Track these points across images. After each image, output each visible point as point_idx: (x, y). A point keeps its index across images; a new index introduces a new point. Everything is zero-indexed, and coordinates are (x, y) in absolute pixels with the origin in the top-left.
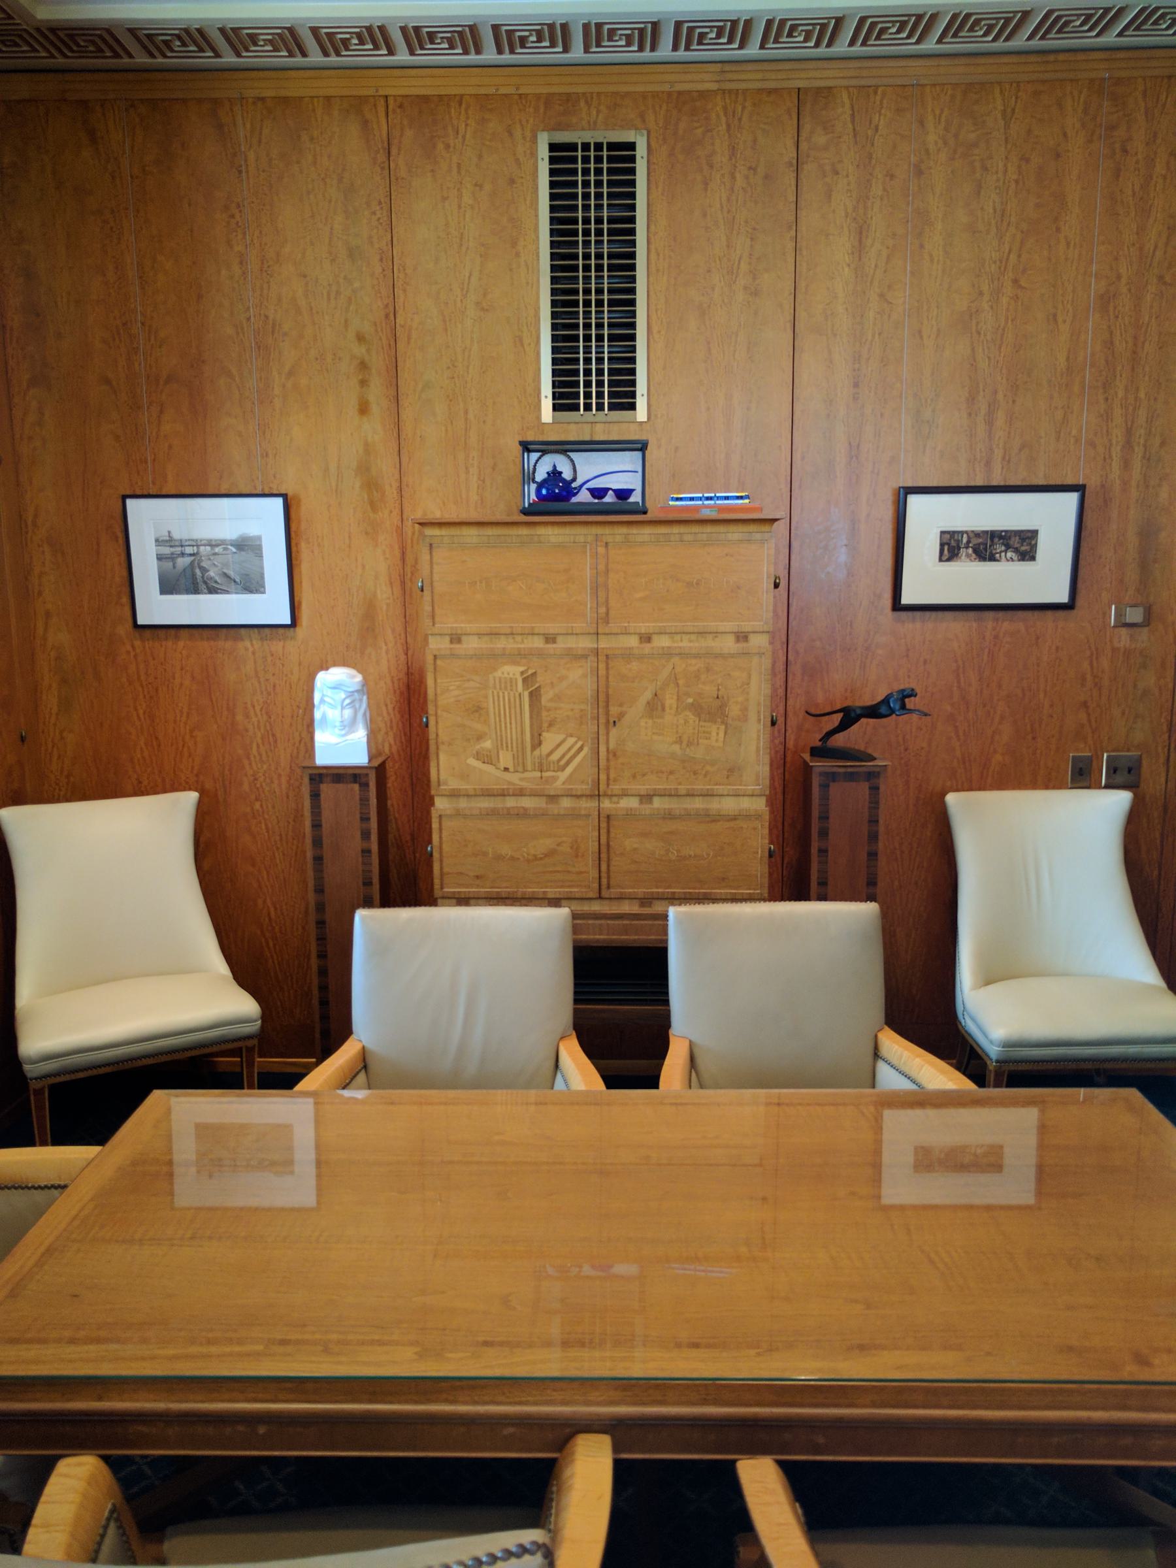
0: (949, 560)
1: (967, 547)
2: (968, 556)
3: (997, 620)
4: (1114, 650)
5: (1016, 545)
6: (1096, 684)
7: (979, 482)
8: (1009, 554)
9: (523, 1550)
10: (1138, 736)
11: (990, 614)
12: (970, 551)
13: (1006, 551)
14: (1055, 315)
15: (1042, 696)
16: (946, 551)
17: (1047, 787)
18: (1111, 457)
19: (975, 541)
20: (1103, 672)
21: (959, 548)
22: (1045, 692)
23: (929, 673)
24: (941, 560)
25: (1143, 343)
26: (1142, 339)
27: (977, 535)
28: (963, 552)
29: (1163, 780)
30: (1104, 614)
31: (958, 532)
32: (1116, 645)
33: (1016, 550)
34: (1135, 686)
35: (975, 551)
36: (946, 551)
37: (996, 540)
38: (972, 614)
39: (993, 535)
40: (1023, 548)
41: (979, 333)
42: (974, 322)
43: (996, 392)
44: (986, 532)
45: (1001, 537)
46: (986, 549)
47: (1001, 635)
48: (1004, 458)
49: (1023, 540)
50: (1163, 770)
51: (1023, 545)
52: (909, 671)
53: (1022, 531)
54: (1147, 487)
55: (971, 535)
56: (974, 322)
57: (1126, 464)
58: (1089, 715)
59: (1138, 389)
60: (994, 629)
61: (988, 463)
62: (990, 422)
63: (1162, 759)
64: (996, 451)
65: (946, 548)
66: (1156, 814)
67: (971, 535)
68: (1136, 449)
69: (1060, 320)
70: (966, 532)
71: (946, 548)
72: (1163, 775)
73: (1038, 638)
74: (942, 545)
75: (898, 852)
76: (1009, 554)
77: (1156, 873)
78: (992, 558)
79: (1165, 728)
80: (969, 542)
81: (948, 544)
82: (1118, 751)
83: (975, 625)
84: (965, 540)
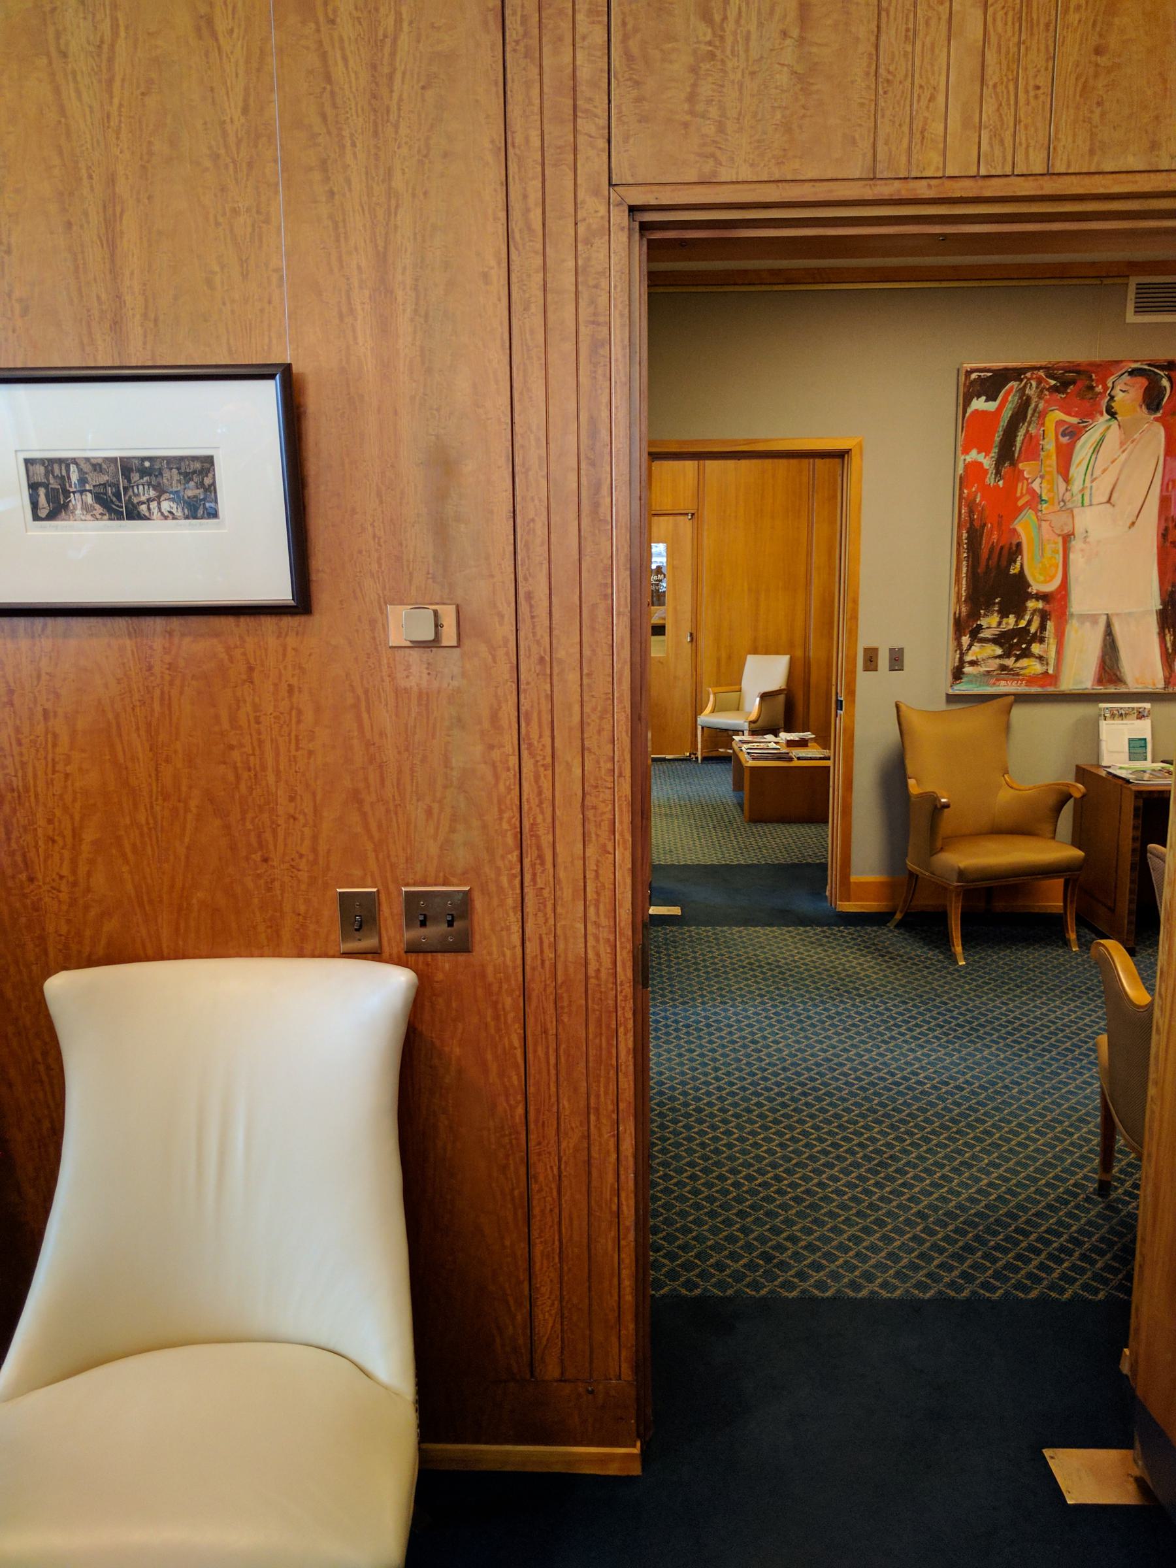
0: (52, 516)
1: (82, 492)
2: (86, 508)
3: (170, 633)
4: (400, 693)
5: (177, 487)
6: (372, 760)
7: (104, 358)
8: (166, 506)
9: (438, 626)
10: (461, 857)
11: (159, 623)
12: (89, 498)
13: (158, 499)
14: (210, 22)
15: (271, 778)
16: (42, 500)
17: (301, 954)
18: (352, 311)
19: (95, 479)
20: (382, 734)
21: (67, 493)
22: (278, 773)
23: (55, 736)
24: (36, 517)
25: (391, 77)
26: (386, 70)
27: (97, 466)
28: (75, 501)
29: (516, 938)
30: (373, 623)
31: (60, 461)
32: (403, 683)
33: (177, 498)
34: (447, 762)
35: (100, 499)
36: (42, 500)
37: (135, 477)
38: (121, 622)
39: (127, 467)
40: (190, 493)
41: (64, 55)
42: (51, 30)
43: (112, 180)
44: (113, 460)
45: (144, 472)
46: (118, 495)
47: (182, 663)
48: (145, 316)
49: (187, 476)
50: (514, 919)
51: (190, 484)
52: (18, 730)
53: (182, 459)
54: (429, 371)
55: (86, 468)
56: (51, 30)
57: (384, 328)
58: (364, 815)
59: (389, 172)
60: (166, 651)
61: (116, 325)
62: (111, 242)
63: (511, 901)
64: (128, 298)
65: (42, 491)
66: (508, 1001)
67: (86, 468)
68: (400, 294)
69: (221, 26)
70: (74, 461)
71: (42, 491)
72: (516, 928)
73: (251, 669)
74: (33, 487)
75: (41, 1068)
76: (166, 506)
77: (520, 1110)
78: (133, 514)
79: (510, 840)
80: (83, 481)
81: (46, 486)
82: (425, 884)
83: (129, 643)
84: (74, 477)
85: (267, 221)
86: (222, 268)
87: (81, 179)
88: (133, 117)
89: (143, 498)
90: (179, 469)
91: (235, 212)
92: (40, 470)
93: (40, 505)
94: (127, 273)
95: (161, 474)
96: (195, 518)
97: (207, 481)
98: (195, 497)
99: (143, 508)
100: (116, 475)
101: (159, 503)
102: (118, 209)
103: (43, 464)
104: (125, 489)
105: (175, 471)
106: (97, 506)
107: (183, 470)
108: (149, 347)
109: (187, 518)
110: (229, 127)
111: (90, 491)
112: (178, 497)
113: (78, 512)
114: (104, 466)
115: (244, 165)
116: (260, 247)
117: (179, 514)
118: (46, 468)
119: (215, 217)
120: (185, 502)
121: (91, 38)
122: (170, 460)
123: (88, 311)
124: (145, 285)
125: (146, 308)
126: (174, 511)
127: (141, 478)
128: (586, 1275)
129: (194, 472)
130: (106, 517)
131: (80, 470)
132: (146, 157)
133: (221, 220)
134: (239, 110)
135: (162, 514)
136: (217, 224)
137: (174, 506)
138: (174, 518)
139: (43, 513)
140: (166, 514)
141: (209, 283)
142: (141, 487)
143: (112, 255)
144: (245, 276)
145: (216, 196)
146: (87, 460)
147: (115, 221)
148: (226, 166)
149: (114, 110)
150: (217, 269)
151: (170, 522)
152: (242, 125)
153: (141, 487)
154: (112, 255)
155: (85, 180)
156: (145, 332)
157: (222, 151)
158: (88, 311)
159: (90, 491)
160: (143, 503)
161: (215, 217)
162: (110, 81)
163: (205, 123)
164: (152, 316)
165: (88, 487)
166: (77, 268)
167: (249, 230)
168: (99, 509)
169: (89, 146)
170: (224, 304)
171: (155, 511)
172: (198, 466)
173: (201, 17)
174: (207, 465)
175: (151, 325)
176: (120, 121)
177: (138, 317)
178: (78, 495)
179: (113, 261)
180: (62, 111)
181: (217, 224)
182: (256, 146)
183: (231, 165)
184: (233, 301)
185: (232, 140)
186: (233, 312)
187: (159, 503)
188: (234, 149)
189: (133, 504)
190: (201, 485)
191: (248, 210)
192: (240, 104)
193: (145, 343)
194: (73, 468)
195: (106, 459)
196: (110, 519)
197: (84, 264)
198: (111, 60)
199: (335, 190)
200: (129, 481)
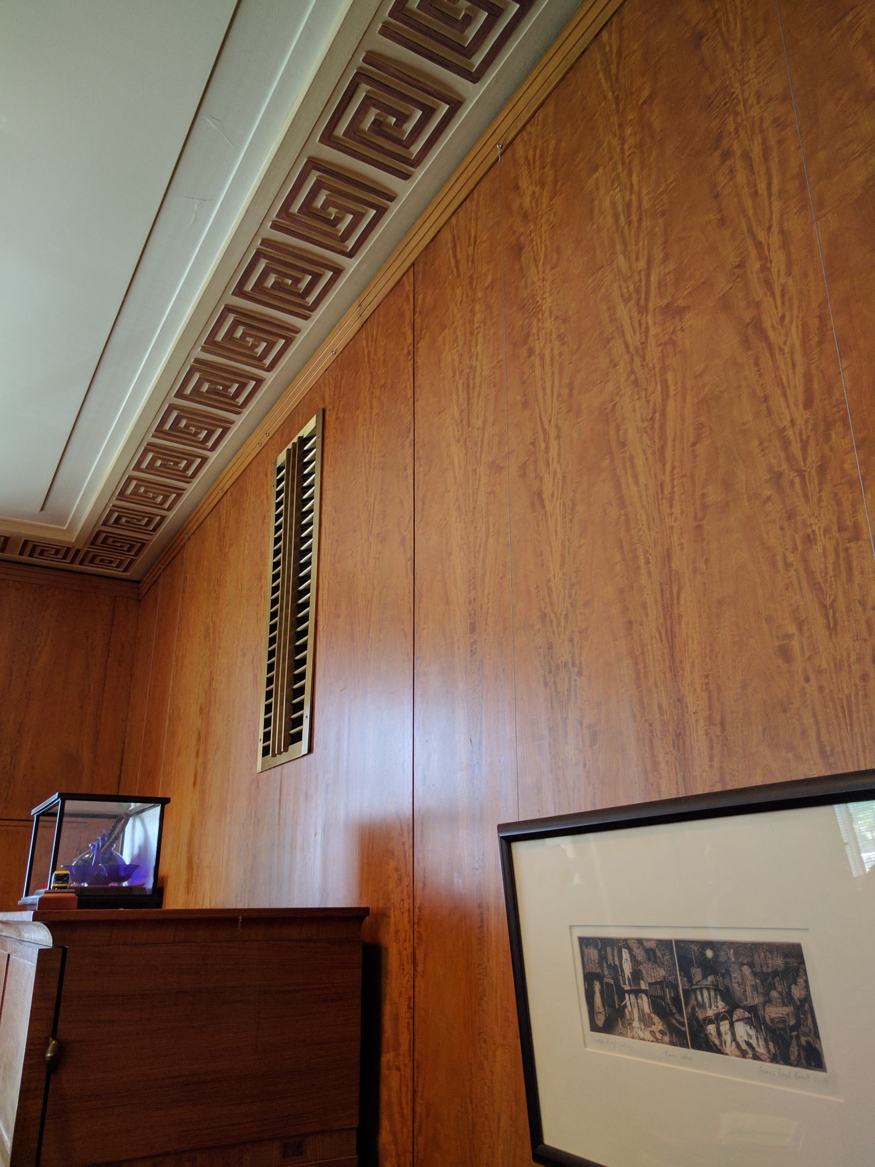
2: (645, 1021)
19: (653, 974)
24: (594, 1028)
33: (755, 1019)
35: (658, 1007)
44: (665, 944)
45: (709, 968)
53: (755, 947)
67: (640, 955)
71: (597, 987)
78: (696, 1037)
80: (637, 975)
85: (856, 537)
86: (800, 626)
87: (639, 567)
88: (685, 476)
89: (710, 1013)
90: (751, 965)
91: (809, 540)
92: (593, 954)
93: (597, 1010)
94: (687, 667)
95: (728, 973)
96: (787, 1061)
97: (797, 993)
98: (783, 1020)
99: (711, 1028)
100: (672, 972)
101: (732, 1025)
102: (675, 589)
103: (596, 947)
104: (687, 993)
105: (746, 969)
106: (656, 1019)
107: (758, 969)
108: (716, 764)
109: (774, 1059)
110: (790, 432)
111: (645, 992)
112: (757, 1016)
113: (636, 1024)
114: (659, 954)
115: (814, 473)
116: (850, 578)
117: (761, 1050)
118: (600, 951)
119: (785, 558)
120: (768, 1028)
121: (645, 415)
122: (739, 948)
123: (650, 725)
124: (707, 676)
125: (710, 708)
126: (754, 1042)
127: (705, 977)
128: (184, 863)
129: (775, 973)
130: (667, 1039)
131: (633, 957)
132: (700, 515)
133: (791, 558)
134: (801, 407)
135: (738, 1046)
136: (788, 565)
137: (752, 1032)
138: (756, 1057)
139: (600, 1020)
140: (744, 1046)
141: (785, 653)
142: (705, 993)
143: (672, 648)
144: (832, 629)
145: (782, 529)
146: (640, 941)
147: (672, 604)
148: (792, 483)
149: (667, 479)
150: (792, 629)
151: (749, 1062)
152: (807, 422)
153: (705, 993)
154: (672, 648)
155: (644, 571)
156: (711, 742)
157: (785, 466)
158: (650, 725)
159: (645, 992)
160: (711, 1022)
161: (785, 558)
162: (662, 449)
163: (761, 443)
164: (717, 718)
165: (643, 986)
166: (638, 678)
167: (831, 558)
168: (658, 1025)
169: (645, 528)
170: (807, 680)
171: (728, 1038)
172: (778, 962)
173: (748, 325)
174: (793, 962)
175: (718, 730)
176: (673, 487)
177: (702, 722)
178: (632, 997)
179: (672, 656)
180: (622, 504)
181: (788, 565)
182: (828, 439)
183: (797, 480)
184: (819, 672)
185: (796, 448)
186: (821, 689)
187: (732, 1025)
188: (800, 457)
189: (697, 1019)
190: (787, 999)
191: (827, 531)
192: (801, 398)
193: (711, 759)
194: (625, 954)
195: (661, 943)
196: (672, 1043)
197: (645, 667)
198: (662, 427)
199: (633, 618)
200: (690, 980)
